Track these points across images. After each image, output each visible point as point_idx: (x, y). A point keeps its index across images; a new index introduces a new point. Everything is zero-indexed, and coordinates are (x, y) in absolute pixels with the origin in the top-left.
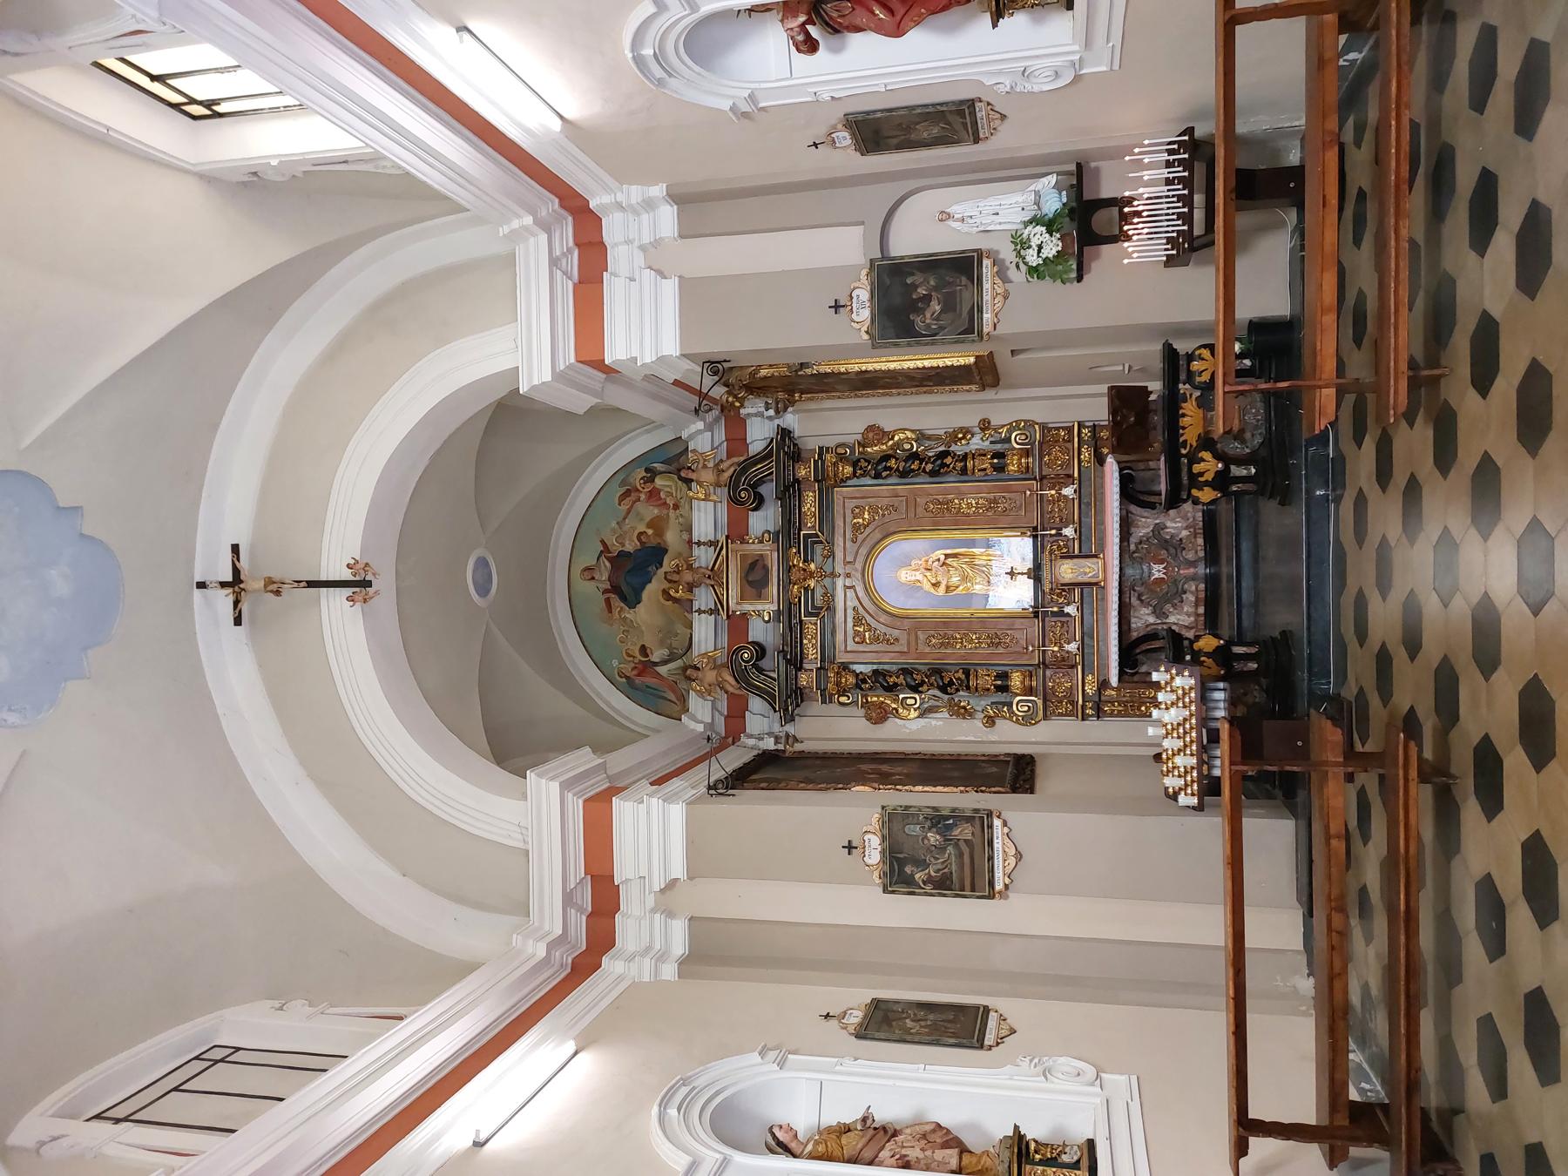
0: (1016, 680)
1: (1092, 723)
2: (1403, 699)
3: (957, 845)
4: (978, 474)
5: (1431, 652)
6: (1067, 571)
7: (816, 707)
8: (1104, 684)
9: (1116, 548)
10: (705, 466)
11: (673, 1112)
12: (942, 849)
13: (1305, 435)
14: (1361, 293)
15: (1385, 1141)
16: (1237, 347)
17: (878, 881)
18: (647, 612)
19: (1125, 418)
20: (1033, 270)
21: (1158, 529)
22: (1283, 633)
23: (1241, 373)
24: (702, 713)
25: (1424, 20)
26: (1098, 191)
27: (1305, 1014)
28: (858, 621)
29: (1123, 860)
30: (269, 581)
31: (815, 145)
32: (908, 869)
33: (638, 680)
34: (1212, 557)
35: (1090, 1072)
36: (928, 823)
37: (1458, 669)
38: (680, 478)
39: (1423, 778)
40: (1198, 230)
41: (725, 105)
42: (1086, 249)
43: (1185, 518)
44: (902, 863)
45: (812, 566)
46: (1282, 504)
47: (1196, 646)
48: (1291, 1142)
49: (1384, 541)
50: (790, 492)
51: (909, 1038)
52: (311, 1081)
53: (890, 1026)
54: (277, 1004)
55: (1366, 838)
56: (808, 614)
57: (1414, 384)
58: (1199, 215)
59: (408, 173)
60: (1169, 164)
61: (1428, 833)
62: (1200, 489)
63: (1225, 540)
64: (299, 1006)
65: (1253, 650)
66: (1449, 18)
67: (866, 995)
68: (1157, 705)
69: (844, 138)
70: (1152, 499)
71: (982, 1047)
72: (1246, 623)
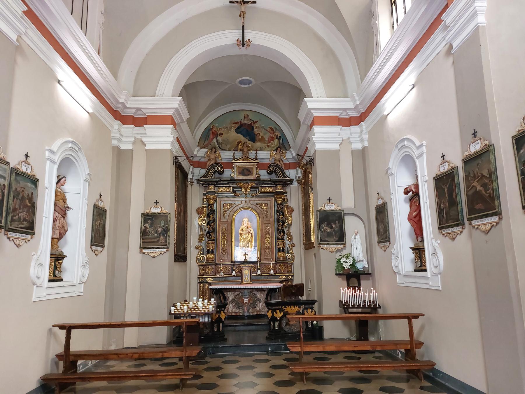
0: (211, 256)
1: (197, 281)
2: (205, 374)
3: (157, 237)
4: (278, 243)
5: (220, 382)
6: (246, 272)
7: (202, 191)
9: (253, 287)
10: (281, 156)
11: (70, 145)
12: (156, 232)
13: (287, 343)
14: (330, 359)
15: (65, 372)
16: (315, 322)
17: (146, 211)
18: (234, 136)
19: (294, 289)
20: (339, 260)
21: (259, 300)
22: (226, 339)
23: (307, 322)
24: (200, 153)
25: (408, 374)
26: (364, 279)
27: (103, 348)
28: (231, 205)
29: (154, 290)
30: (244, 13)
31: (378, 193)
32: (149, 221)
33: (211, 132)
34: (250, 317)
35: (84, 280)
36: (165, 228)
37: (215, 389)
38: (277, 148)
39: (181, 380)
40: (350, 310)
41: (390, 166)
42: (345, 276)
43: (263, 309)
44: (152, 219)
45: (249, 190)
46: (267, 338)
47: (222, 312)
48: (64, 343)
49: (254, 368)
50: (273, 183)
51: (94, 222)
52: (78, 25)
53: (98, 216)
54: (103, 12)
55: (161, 365)
56: (233, 189)
57: (301, 374)
58: (355, 310)
59: (373, 64)
60: (370, 301)
61: (164, 382)
62: (271, 312)
63: (255, 321)
64: (102, 19)
65: (221, 330)
66: (408, 381)
67: (107, 208)
68: (203, 300)
69: (380, 202)
70: (269, 298)
71: (91, 245)
72: (229, 328)
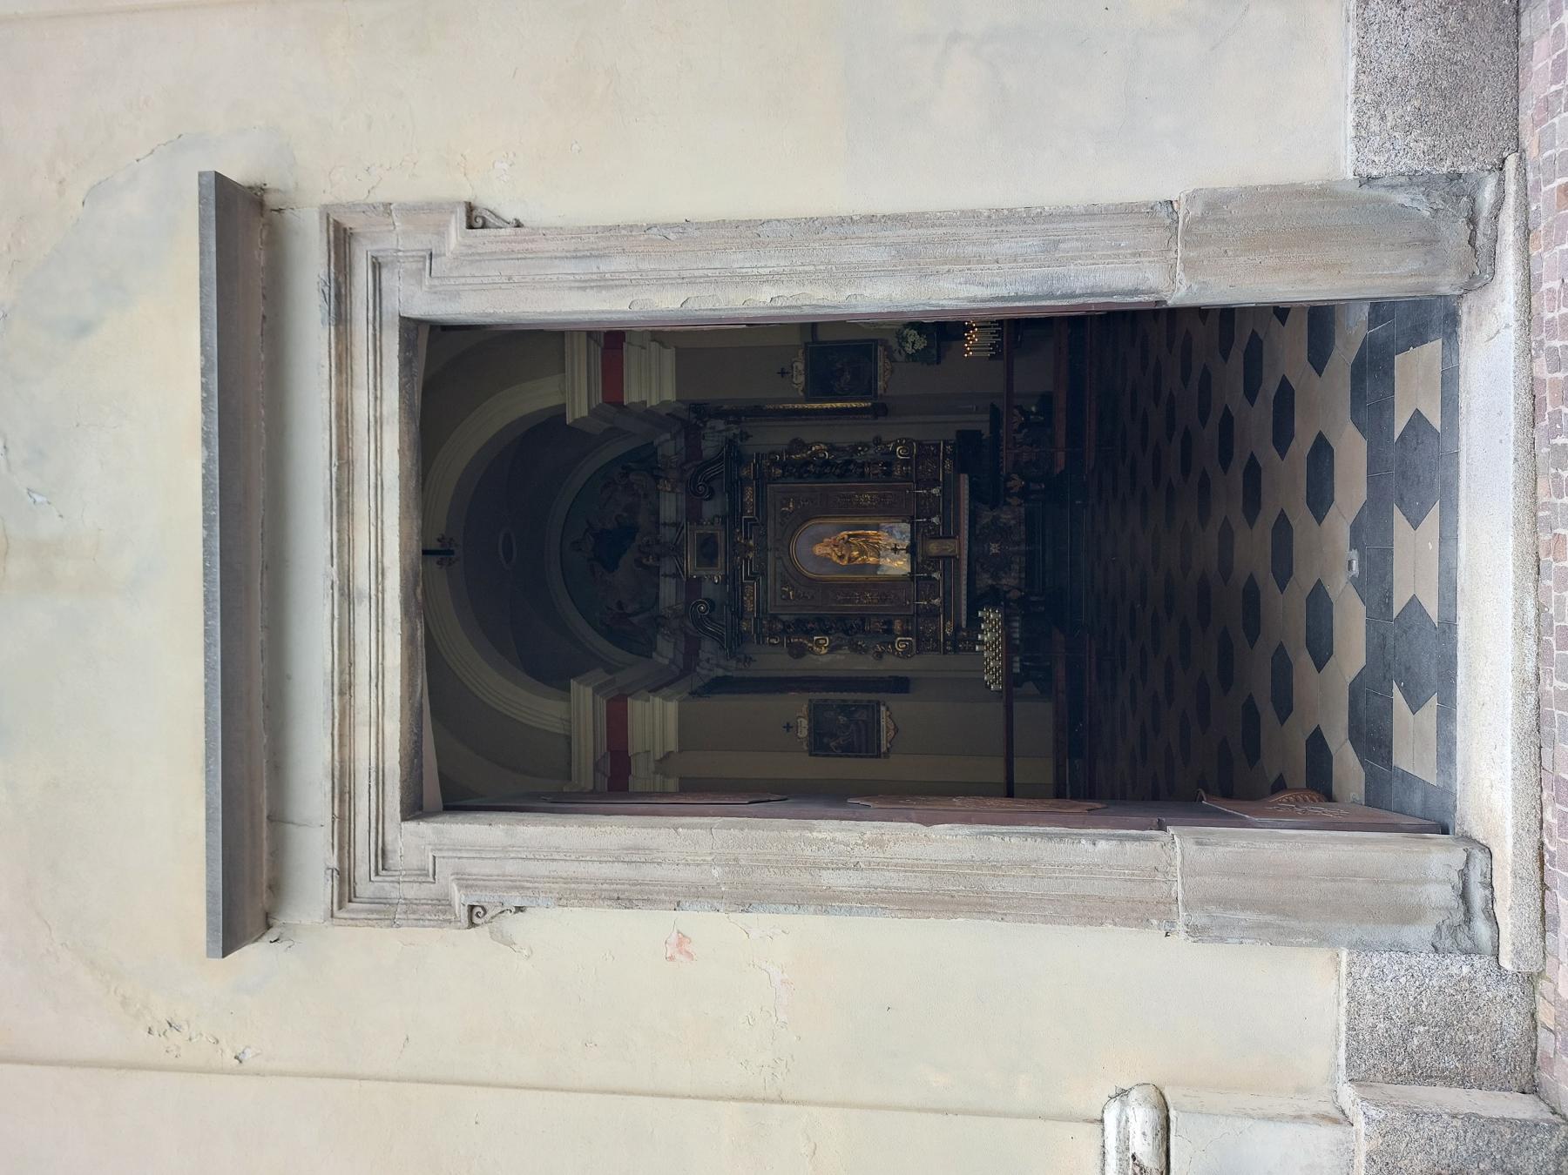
0: (897, 626)
6: (934, 548)
8: (957, 628)
68: (982, 632)
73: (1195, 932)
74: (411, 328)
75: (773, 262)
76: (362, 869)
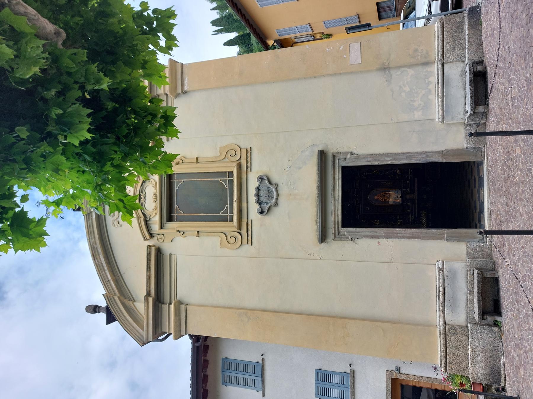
0: (398, 217)
6: (408, 197)
73: (447, 240)
74: (344, 168)
75: (391, 158)
76: (337, 234)
